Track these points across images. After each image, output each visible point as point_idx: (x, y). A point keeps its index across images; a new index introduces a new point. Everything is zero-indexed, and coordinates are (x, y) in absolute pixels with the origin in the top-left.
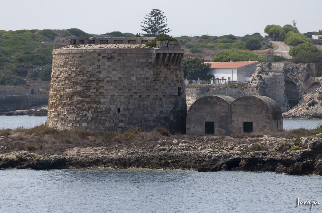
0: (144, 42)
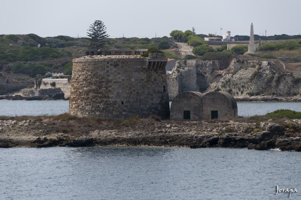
0: (137, 53)
